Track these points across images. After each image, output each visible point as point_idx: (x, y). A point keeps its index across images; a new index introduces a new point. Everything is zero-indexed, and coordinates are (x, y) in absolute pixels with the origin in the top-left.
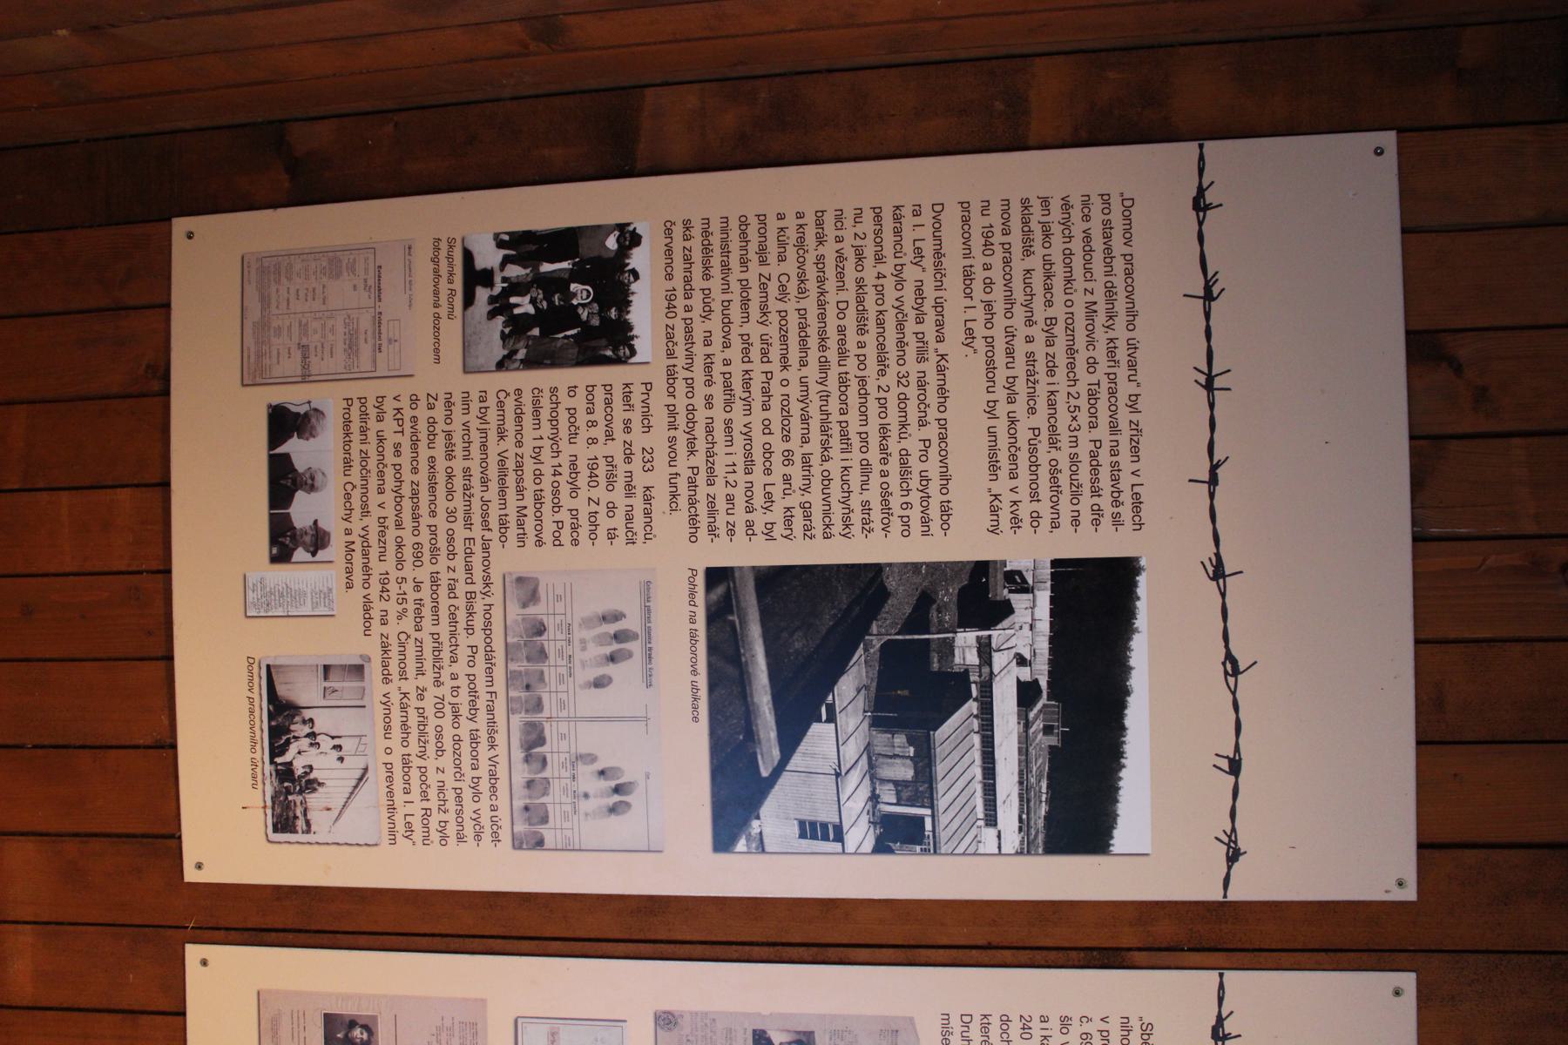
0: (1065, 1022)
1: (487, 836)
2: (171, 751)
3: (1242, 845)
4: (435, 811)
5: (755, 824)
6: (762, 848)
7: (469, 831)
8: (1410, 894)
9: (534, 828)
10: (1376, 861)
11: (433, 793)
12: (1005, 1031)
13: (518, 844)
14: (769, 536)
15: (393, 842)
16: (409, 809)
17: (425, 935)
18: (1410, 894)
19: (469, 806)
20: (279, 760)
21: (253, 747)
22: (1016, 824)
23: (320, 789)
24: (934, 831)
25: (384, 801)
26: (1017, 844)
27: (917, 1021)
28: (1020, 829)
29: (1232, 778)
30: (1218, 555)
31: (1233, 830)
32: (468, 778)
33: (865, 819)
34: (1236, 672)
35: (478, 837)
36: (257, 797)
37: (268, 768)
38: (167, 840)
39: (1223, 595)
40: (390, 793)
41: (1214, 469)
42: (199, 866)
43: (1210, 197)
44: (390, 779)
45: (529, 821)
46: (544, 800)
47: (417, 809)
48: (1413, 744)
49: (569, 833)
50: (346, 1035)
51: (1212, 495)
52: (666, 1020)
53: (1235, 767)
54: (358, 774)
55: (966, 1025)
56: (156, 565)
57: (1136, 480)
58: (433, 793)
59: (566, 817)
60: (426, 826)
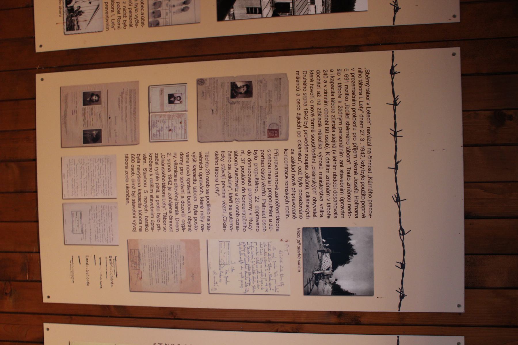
0: (339, 71)
1: (140, 24)
3: (405, 293)
4: (122, 17)
5: (232, 10)
6: (234, 18)
7: (134, 23)
8: (457, 20)
9: (156, 19)
10: (451, 298)
11: (121, 11)
12: (318, 76)
13: (150, 25)
15: (108, 29)
16: (113, 17)
17: (118, 62)
18: (457, 20)
19: (134, 14)
20: (69, 6)
21: (60, 2)
22: (321, 3)
23: (83, 14)
24: (293, 7)
25: (105, 15)
26: (322, 10)
27: (288, 76)
28: (323, 5)
30: (398, 194)
31: (402, 288)
32: (133, 5)
33: (269, 5)
34: (404, 234)
35: (137, 24)
36: (61, 20)
37: (65, 9)
38: (30, 39)
39: (399, 207)
40: (107, 13)
41: (396, 164)
42: (42, 80)
43: (396, 69)
44: (107, 8)
45: (154, 17)
46: (159, 9)
47: (116, 17)
48: (460, 75)
49: (168, 20)
50: (90, 99)
51: (396, 173)
52: (200, 82)
53: (403, 266)
54: (96, 7)
55: (305, 75)
56: (36, 220)
57: (368, 106)
58: (121, 11)
59: (167, 14)
60: (119, 23)
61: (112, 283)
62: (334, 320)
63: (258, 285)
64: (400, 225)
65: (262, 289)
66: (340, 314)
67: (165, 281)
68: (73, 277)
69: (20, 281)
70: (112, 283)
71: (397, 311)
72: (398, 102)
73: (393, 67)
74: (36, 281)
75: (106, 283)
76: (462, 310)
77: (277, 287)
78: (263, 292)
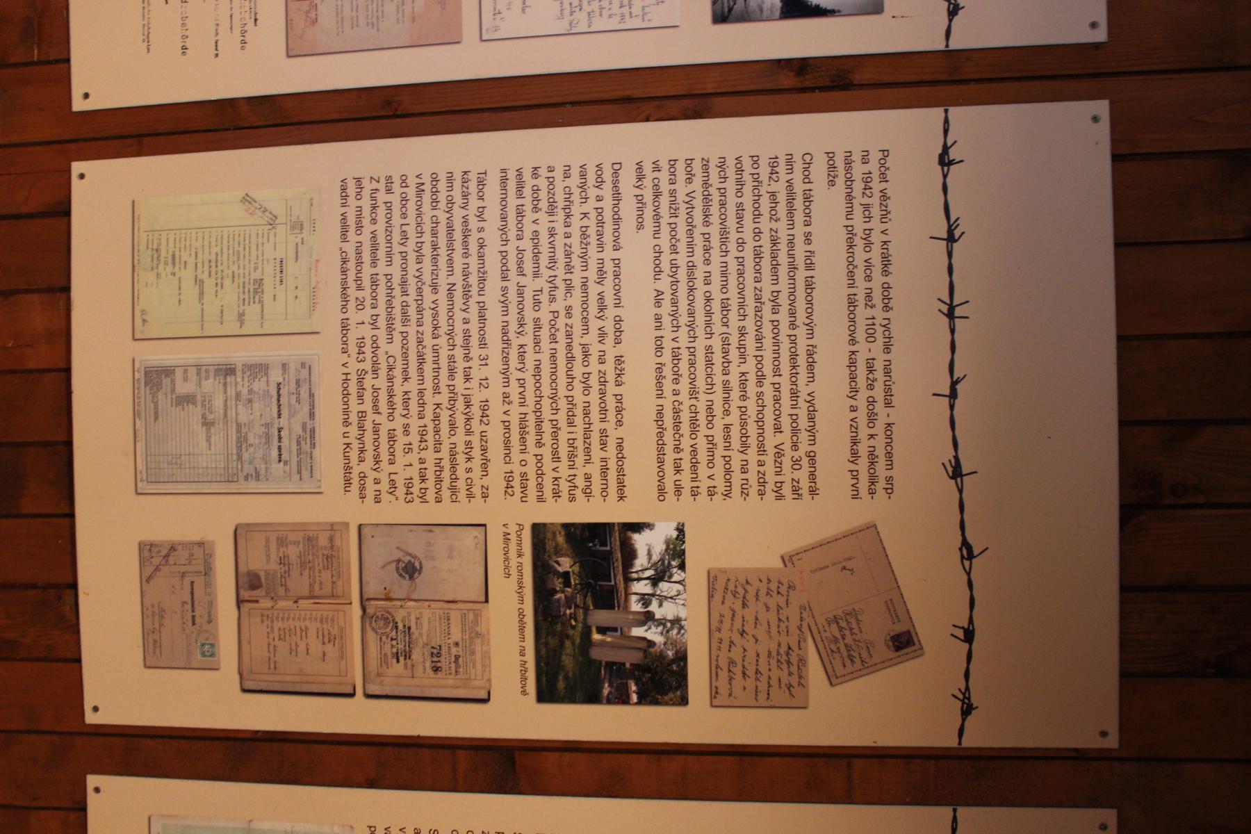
2: (66, 521)
10: (1086, 713)
14: (588, 493)
29: (966, 646)
30: (956, 458)
31: (967, 688)
34: (971, 556)
39: (961, 491)
41: (954, 384)
43: (953, 154)
51: (952, 407)
53: (969, 636)
56: (67, 511)
61: (243, 42)
62: (787, 80)
63: (601, 8)
64: (963, 535)
65: (610, 16)
66: (801, 66)
67: (375, 20)
68: (147, 39)
69: (15, 65)
70: (243, 42)
71: (942, 47)
72: (957, 233)
73: (946, 149)
74: (58, 61)
75: (230, 41)
76: (1101, 35)
77: (647, 10)
78: (614, 24)
